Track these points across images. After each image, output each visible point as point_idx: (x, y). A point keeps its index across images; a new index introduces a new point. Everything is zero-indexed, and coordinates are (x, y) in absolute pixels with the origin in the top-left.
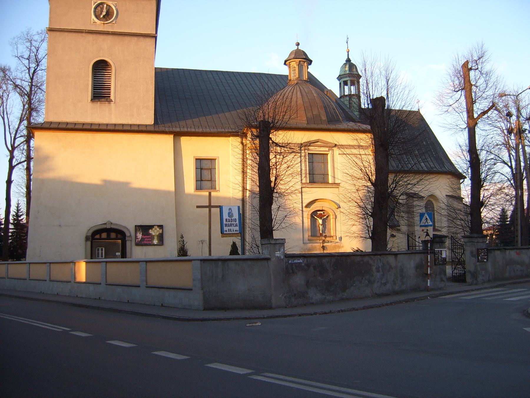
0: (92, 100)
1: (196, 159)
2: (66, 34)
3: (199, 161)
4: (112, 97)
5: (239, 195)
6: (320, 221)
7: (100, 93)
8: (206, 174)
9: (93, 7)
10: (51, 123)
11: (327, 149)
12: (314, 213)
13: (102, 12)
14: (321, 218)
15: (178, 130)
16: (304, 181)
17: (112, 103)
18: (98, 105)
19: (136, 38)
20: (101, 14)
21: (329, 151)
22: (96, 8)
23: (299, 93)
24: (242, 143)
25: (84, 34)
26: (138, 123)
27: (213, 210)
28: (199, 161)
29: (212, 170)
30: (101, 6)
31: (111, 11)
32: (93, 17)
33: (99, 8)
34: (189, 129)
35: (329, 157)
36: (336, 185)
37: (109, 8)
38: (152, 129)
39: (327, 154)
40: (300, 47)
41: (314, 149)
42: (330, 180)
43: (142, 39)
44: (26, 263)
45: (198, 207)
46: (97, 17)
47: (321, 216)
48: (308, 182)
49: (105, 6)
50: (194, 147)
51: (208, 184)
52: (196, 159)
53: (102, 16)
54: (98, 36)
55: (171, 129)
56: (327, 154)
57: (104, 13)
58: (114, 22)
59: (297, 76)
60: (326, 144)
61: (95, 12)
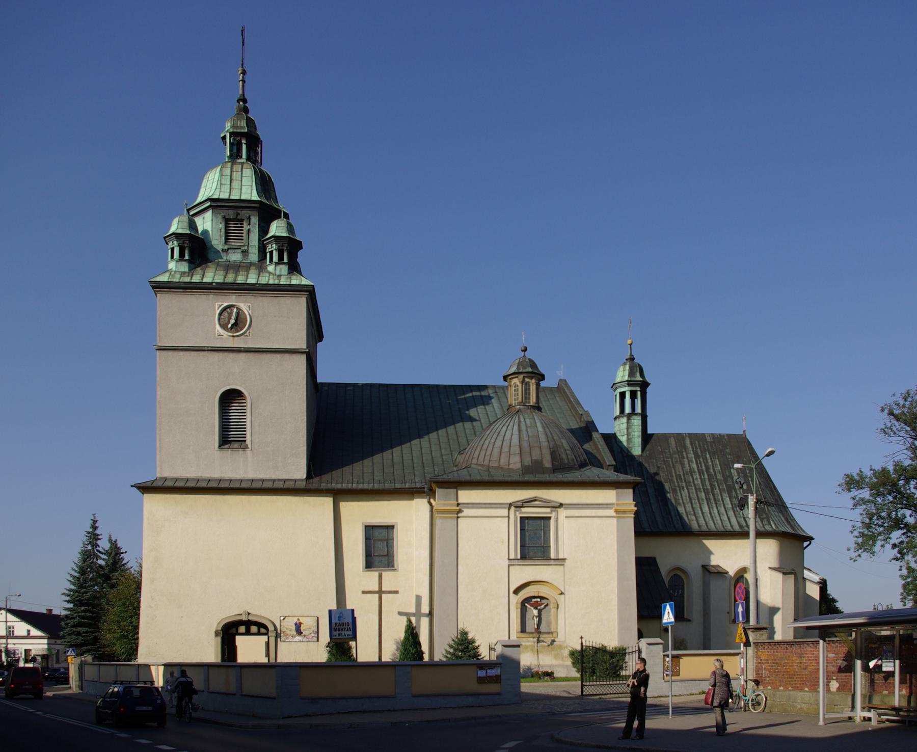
0: (220, 446)
1: (366, 527)
2: (181, 353)
3: (370, 530)
4: (248, 442)
5: (615, 520)
6: (535, 612)
7: (229, 437)
8: (380, 548)
9: (218, 312)
10: (166, 479)
11: (548, 510)
12: (528, 600)
13: (230, 318)
14: (536, 608)
15: (339, 486)
16: (512, 556)
17: (248, 452)
18: (228, 453)
19: (278, 356)
20: (229, 322)
21: (551, 513)
22: (220, 314)
23: (516, 427)
24: (431, 504)
25: (205, 353)
26: (284, 477)
27: (384, 596)
28: (370, 530)
29: (389, 543)
30: (228, 310)
31: (242, 317)
32: (218, 327)
33: (226, 314)
34: (354, 486)
35: (552, 522)
36: (561, 561)
37: (239, 313)
38: (302, 485)
39: (550, 518)
40: (528, 355)
41: (529, 511)
42: (553, 556)
43: (287, 356)
44: (235, 666)
45: (364, 592)
46: (224, 326)
47: (536, 606)
48: (519, 557)
49: (235, 310)
50: (360, 514)
51: (385, 560)
52: (366, 527)
53: (230, 326)
54: (226, 354)
55: (329, 486)
56: (550, 518)
57: (232, 321)
58: (247, 334)
59: (520, 400)
60: (546, 504)
61: (219, 319)
